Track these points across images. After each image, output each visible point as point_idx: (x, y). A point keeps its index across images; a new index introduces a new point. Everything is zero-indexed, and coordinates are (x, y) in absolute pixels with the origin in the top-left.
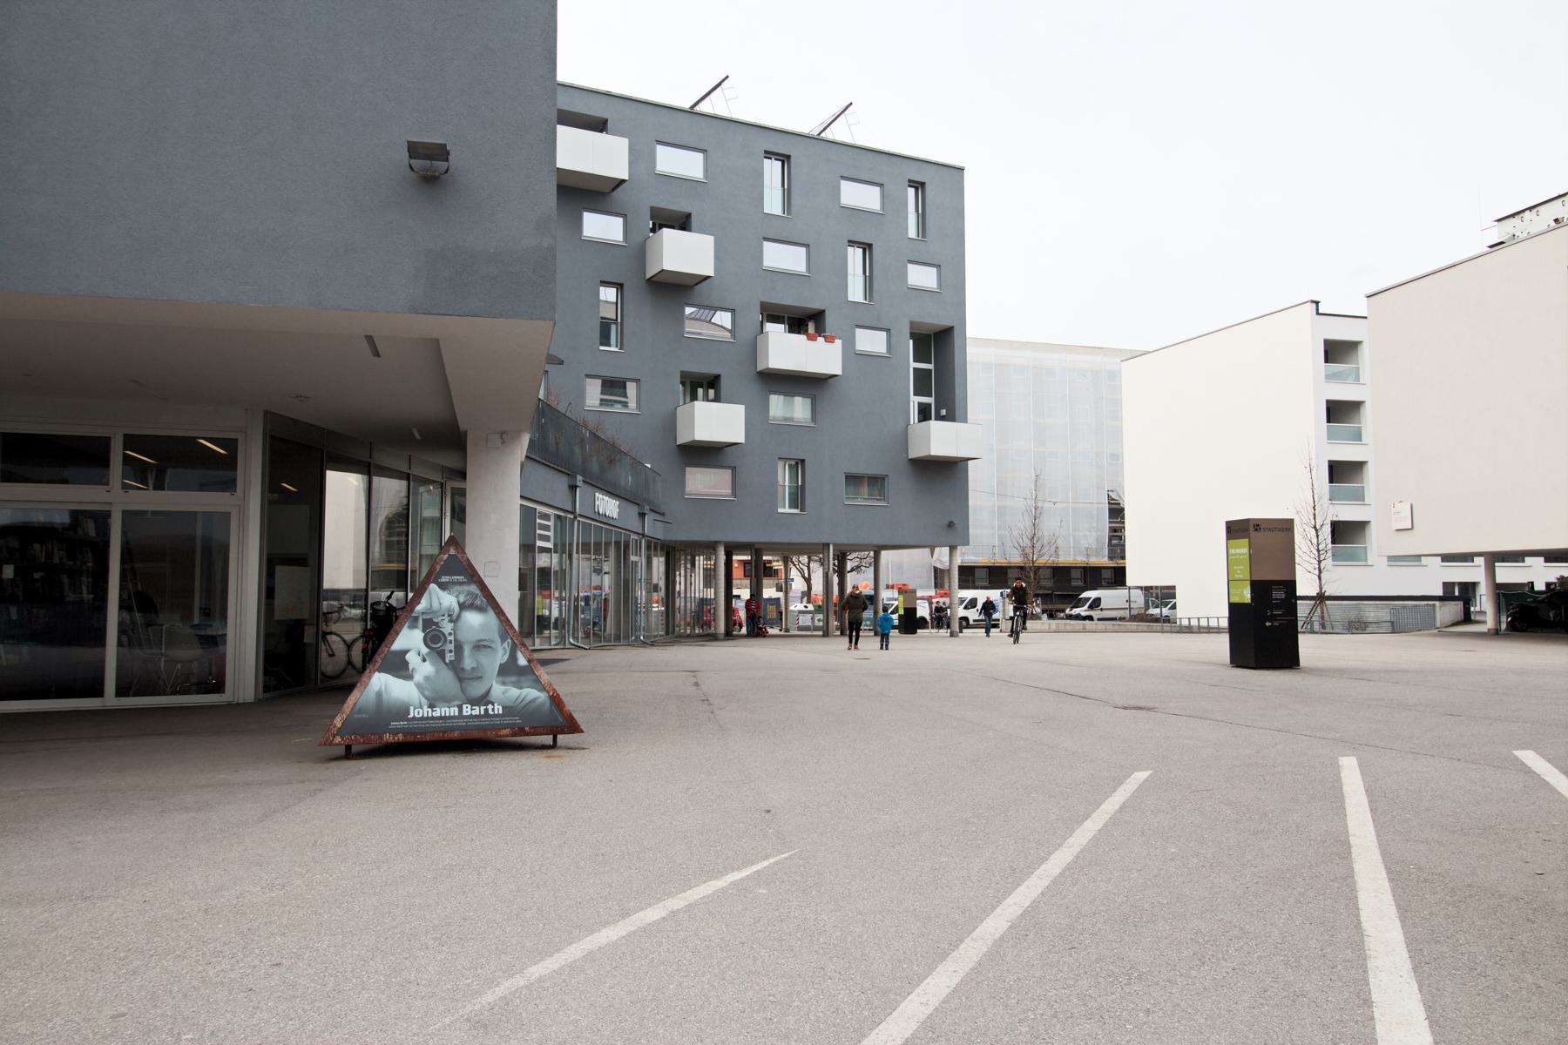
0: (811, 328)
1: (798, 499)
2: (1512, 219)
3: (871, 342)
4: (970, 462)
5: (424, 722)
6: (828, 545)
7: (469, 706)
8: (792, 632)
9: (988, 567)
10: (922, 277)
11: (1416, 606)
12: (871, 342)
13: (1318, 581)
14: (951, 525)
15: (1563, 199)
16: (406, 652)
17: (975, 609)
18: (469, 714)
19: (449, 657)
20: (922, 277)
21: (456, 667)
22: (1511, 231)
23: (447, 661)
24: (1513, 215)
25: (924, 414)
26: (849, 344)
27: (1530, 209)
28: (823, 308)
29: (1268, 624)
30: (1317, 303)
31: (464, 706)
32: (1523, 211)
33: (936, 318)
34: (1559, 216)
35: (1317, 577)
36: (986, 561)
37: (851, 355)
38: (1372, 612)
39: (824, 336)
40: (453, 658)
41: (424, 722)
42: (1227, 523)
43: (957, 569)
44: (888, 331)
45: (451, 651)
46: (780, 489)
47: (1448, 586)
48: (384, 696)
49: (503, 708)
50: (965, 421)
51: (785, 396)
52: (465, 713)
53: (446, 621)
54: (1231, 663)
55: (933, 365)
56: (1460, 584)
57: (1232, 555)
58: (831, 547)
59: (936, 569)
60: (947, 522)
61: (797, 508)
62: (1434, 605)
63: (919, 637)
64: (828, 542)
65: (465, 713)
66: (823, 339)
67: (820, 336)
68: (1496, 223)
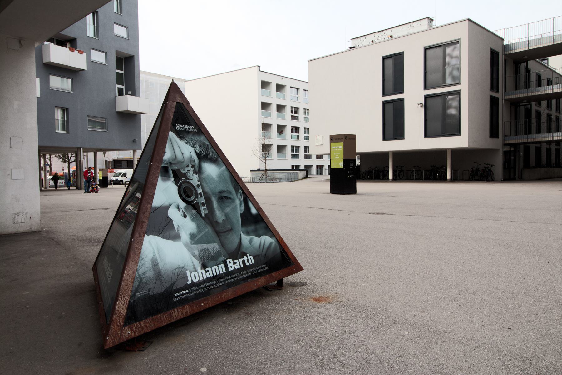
0: (69, 45)
1: (66, 126)
2: (356, 39)
3: (99, 57)
4: (142, 115)
5: (202, 286)
6: (80, 148)
7: (231, 260)
8: (49, 189)
9: (127, 160)
10: (120, 31)
11: (293, 172)
12: (99, 57)
13: (265, 164)
14: (134, 141)
15: (375, 34)
16: (167, 208)
17: (126, 177)
18: (233, 269)
19: (204, 210)
20: (120, 31)
21: (210, 219)
22: (356, 43)
23: (203, 215)
24: (357, 38)
25: (120, 93)
26: (89, 56)
27: (363, 36)
28: (76, 37)
29: (348, 176)
30: (259, 67)
31: (228, 261)
32: (361, 37)
33: (127, 50)
34: (373, 40)
35: (264, 163)
36: (128, 158)
37: (91, 62)
38: (278, 175)
39: (77, 50)
40: (207, 212)
41: (202, 286)
42: (355, 136)
43: (136, 161)
44: (106, 53)
45: (203, 204)
46: (56, 121)
47: (293, 166)
48: (161, 265)
49: (254, 257)
50: (139, 96)
51: (61, 77)
52: (230, 269)
53: (191, 172)
54: (331, 192)
55: (124, 72)
56: (320, 165)
57: (332, 149)
58: (82, 149)
59: (106, 161)
60: (133, 140)
61: (65, 131)
62: (298, 172)
63: (109, 189)
64: (80, 147)
65: (230, 269)
66: (77, 51)
67: (76, 50)
68: (351, 40)
